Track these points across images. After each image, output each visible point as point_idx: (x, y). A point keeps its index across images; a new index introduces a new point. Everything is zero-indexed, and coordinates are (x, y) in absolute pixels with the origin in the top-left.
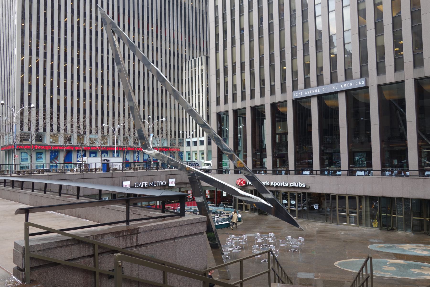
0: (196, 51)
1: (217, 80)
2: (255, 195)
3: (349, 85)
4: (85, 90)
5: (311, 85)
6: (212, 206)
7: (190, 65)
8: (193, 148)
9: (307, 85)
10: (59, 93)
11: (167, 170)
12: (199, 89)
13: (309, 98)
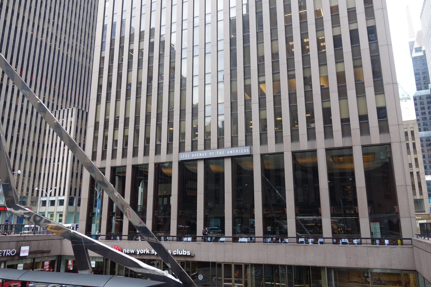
0: (66, 102)
1: (94, 133)
2: (157, 267)
3: (235, 152)
5: (199, 148)
8: (49, 208)
9: (194, 147)
11: (19, 235)
13: (195, 161)
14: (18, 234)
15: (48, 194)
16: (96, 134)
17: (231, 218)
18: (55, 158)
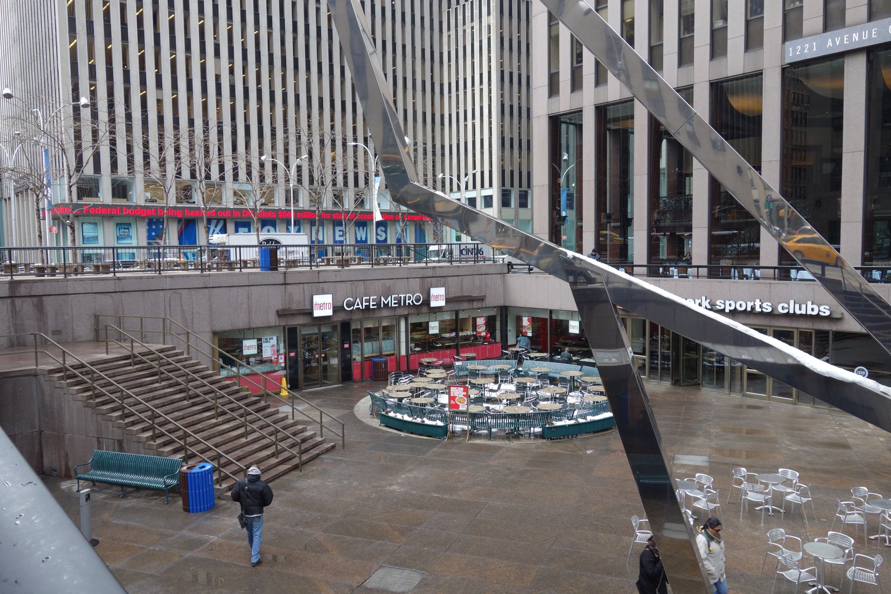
1: (550, 26)
4: (218, 77)
5: (849, 18)
6: (543, 359)
7: (460, 17)
10: (159, 85)
11: (424, 265)
12: (481, 75)
13: (834, 61)
14: (419, 262)
15: (463, 186)
16: (553, 28)
17: (861, 220)
18: (465, 112)
